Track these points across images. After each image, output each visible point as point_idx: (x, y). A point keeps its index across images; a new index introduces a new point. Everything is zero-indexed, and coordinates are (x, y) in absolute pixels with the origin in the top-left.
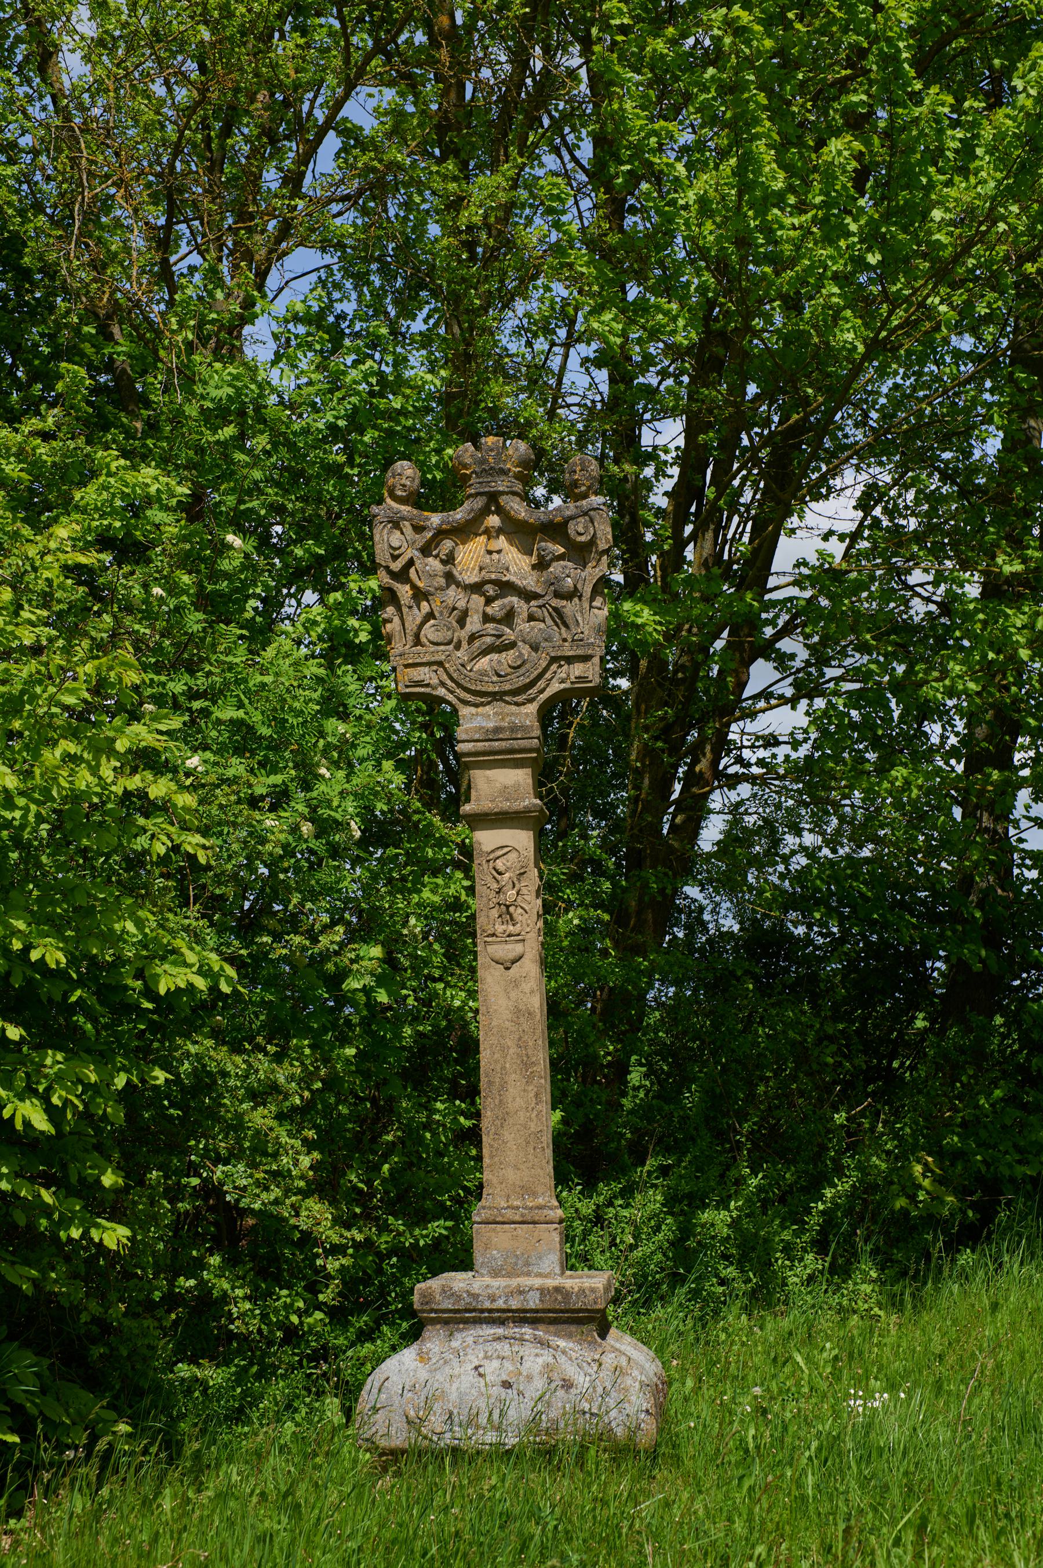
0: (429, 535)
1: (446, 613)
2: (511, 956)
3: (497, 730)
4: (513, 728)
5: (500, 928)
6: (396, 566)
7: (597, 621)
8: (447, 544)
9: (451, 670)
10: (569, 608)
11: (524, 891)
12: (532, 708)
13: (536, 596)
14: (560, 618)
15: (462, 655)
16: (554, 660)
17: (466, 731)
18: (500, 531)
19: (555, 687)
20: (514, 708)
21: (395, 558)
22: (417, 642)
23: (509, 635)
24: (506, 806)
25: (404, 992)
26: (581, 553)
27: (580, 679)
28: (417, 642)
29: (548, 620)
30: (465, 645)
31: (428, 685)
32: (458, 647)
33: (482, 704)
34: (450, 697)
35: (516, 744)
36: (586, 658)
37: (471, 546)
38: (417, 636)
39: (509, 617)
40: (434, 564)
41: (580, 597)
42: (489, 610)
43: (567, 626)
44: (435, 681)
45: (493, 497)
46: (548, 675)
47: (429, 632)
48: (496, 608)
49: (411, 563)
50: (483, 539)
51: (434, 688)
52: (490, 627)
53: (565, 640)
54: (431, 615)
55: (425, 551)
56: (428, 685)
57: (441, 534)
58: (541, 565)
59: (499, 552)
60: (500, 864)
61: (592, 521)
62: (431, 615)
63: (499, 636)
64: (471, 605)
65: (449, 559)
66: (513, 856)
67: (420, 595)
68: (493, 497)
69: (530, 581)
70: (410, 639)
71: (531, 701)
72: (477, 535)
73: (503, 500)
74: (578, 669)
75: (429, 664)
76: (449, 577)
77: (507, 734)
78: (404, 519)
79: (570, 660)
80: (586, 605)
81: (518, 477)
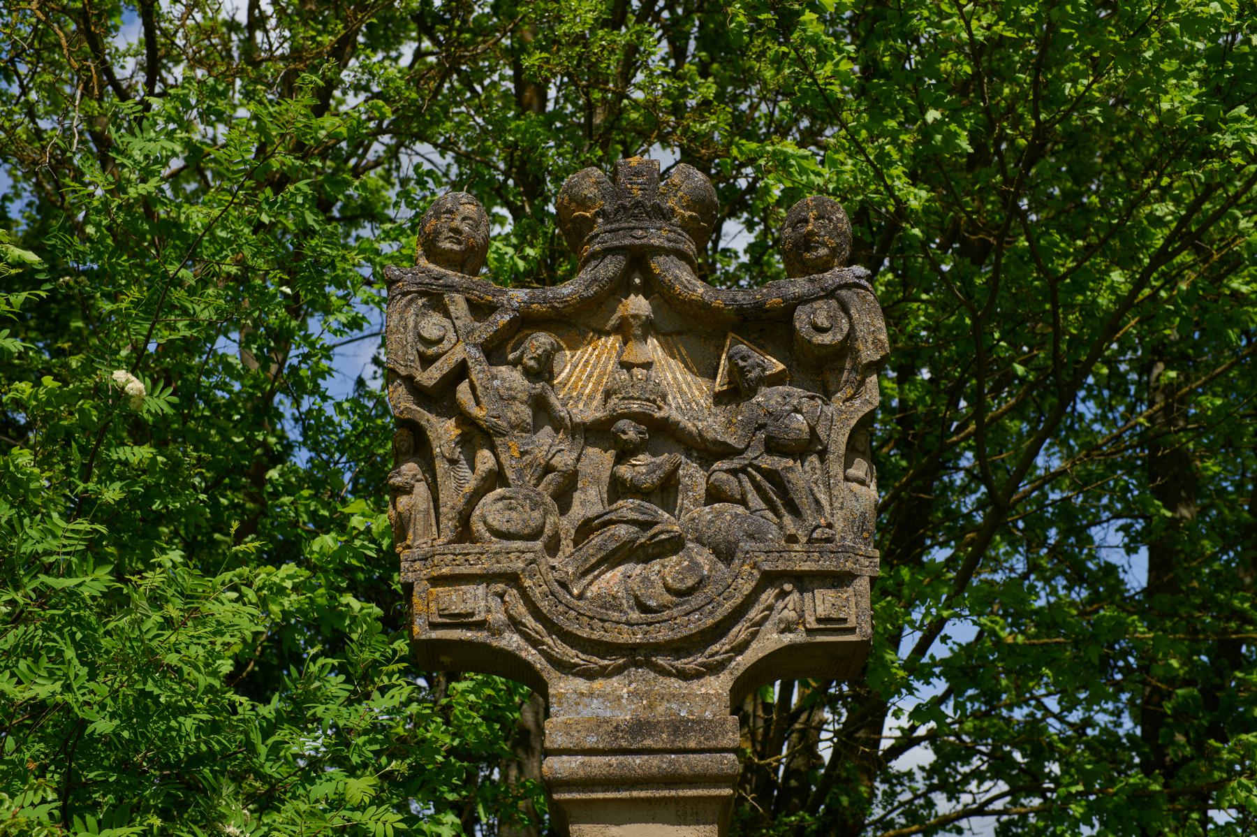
0: (503, 319)
1: (530, 479)
3: (640, 727)
4: (678, 727)
6: (430, 377)
7: (859, 508)
8: (542, 340)
9: (536, 594)
10: (801, 474)
12: (718, 686)
13: (727, 452)
14: (781, 495)
15: (565, 562)
16: (769, 579)
17: (567, 728)
18: (650, 328)
19: (771, 641)
20: (675, 684)
21: (427, 361)
22: (465, 533)
23: (669, 524)
26: (820, 368)
27: (830, 623)
28: (465, 533)
29: (754, 500)
30: (567, 546)
31: (481, 625)
32: (553, 547)
33: (604, 673)
34: (531, 655)
35: (685, 764)
36: (839, 580)
37: (587, 353)
38: (464, 519)
39: (665, 490)
40: (512, 377)
41: (823, 455)
42: (625, 471)
43: (796, 512)
44: (498, 616)
45: (638, 259)
46: (754, 613)
47: (491, 510)
48: (641, 467)
49: (461, 371)
50: (613, 341)
51: (496, 632)
52: (628, 507)
53: (792, 539)
54: (496, 478)
55: (494, 351)
56: (481, 625)
57: (526, 322)
58: (737, 391)
59: (648, 366)
61: (845, 308)
62: (496, 478)
63: (645, 526)
64: (585, 467)
65: (542, 371)
67: (476, 435)
68: (638, 259)
69: (713, 424)
70: (448, 524)
71: (715, 669)
72: (601, 333)
73: (658, 264)
74: (823, 602)
75: (487, 578)
76: (540, 406)
77: (662, 741)
78: (452, 288)
79: (804, 581)
80: (836, 469)
81: (686, 226)
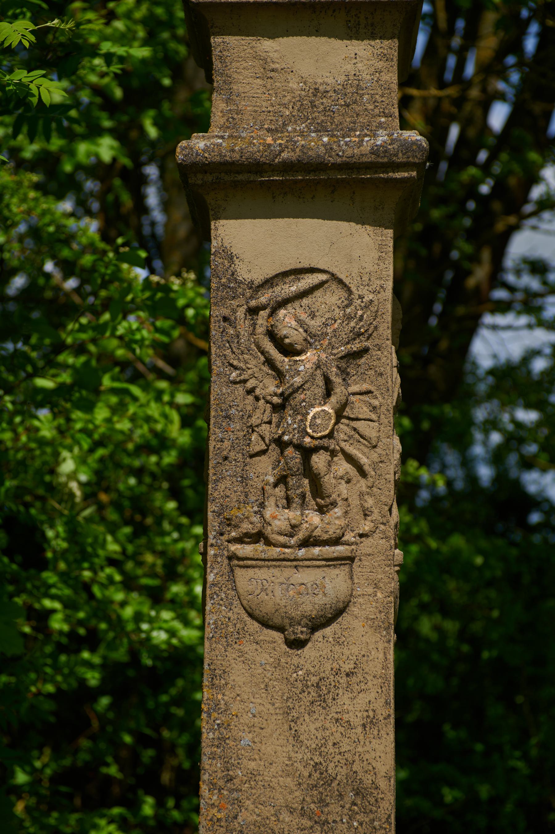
2: (311, 605)
5: (279, 518)
11: (359, 407)
24: (317, 144)
25: (48, 603)
60: (288, 322)
66: (329, 300)
